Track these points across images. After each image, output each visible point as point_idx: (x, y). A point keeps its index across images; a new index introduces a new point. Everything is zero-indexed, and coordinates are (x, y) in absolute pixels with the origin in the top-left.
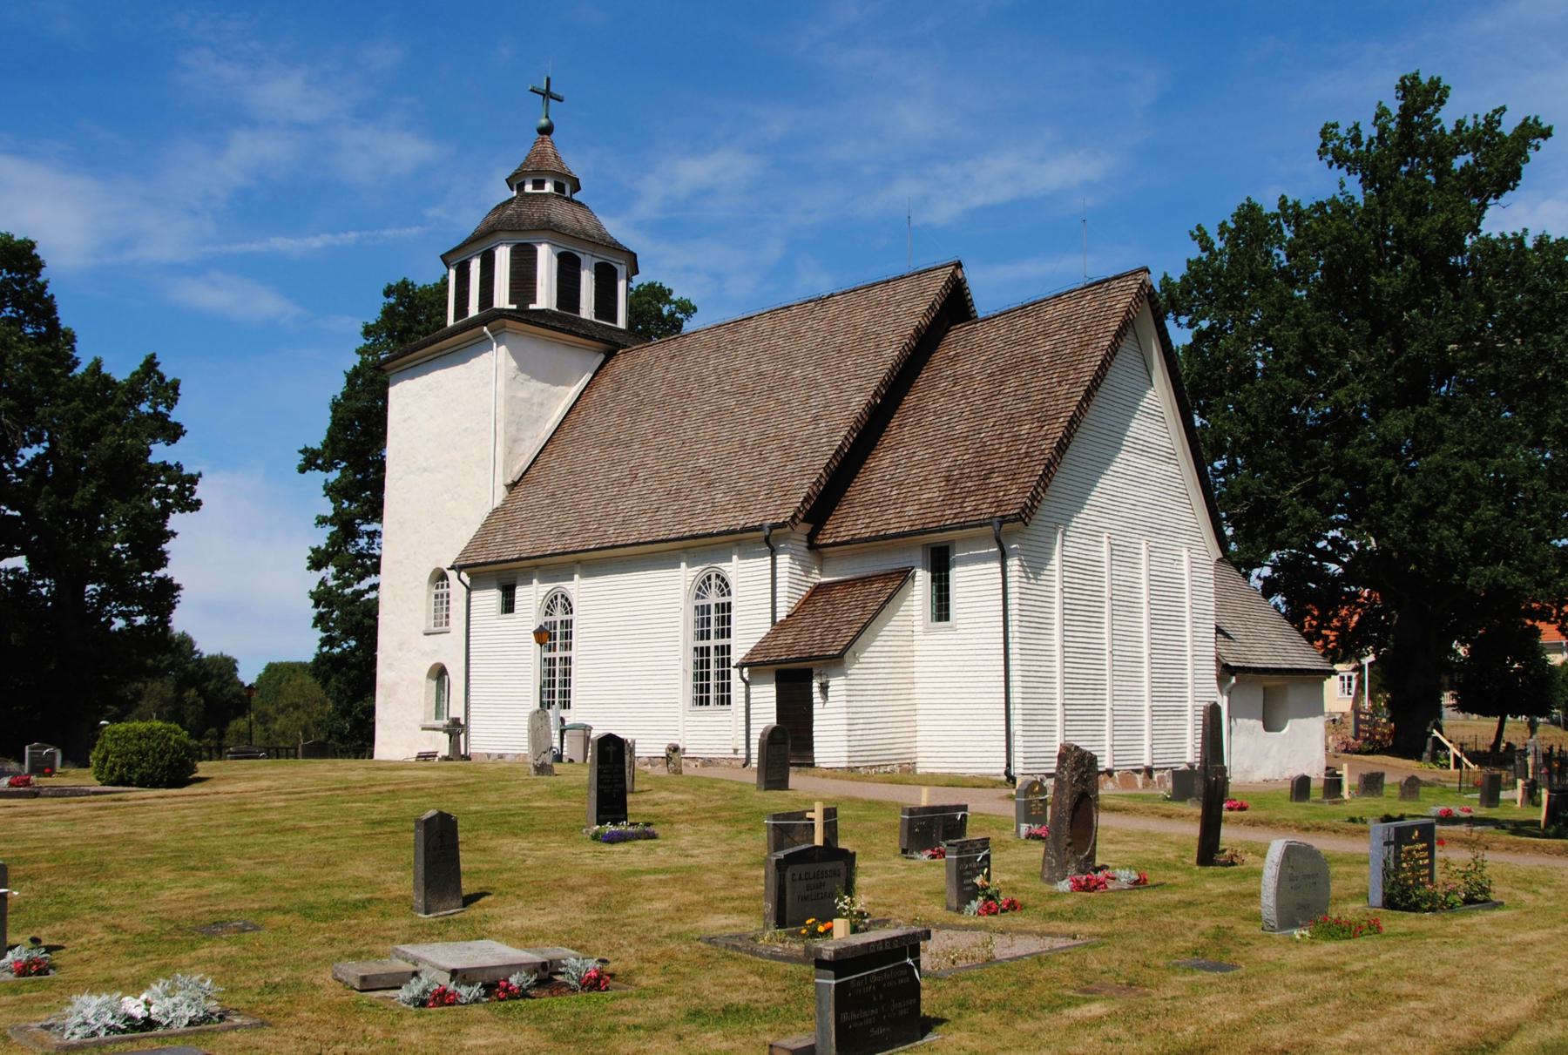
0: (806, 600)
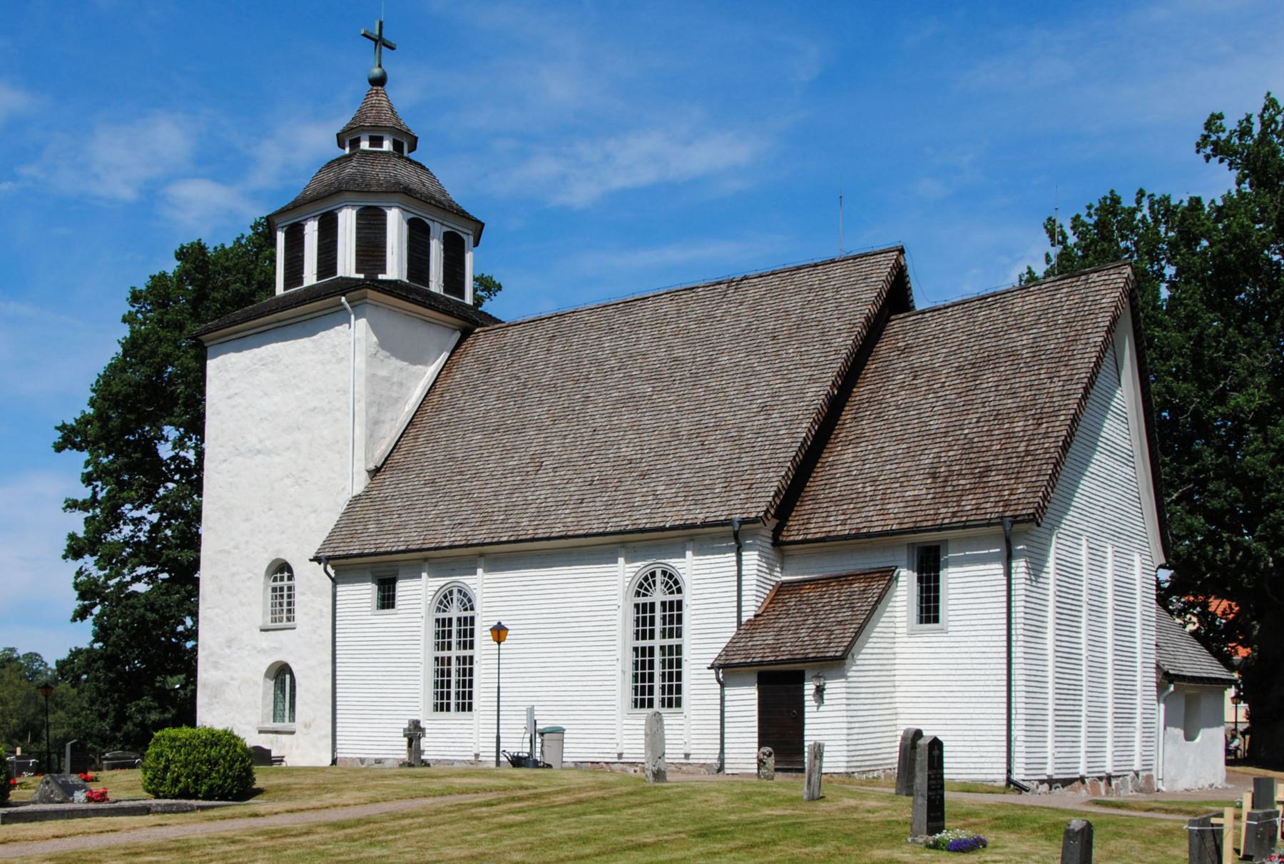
0: (773, 599)
